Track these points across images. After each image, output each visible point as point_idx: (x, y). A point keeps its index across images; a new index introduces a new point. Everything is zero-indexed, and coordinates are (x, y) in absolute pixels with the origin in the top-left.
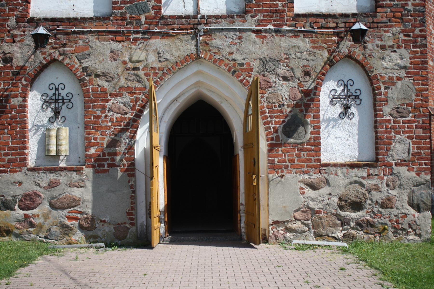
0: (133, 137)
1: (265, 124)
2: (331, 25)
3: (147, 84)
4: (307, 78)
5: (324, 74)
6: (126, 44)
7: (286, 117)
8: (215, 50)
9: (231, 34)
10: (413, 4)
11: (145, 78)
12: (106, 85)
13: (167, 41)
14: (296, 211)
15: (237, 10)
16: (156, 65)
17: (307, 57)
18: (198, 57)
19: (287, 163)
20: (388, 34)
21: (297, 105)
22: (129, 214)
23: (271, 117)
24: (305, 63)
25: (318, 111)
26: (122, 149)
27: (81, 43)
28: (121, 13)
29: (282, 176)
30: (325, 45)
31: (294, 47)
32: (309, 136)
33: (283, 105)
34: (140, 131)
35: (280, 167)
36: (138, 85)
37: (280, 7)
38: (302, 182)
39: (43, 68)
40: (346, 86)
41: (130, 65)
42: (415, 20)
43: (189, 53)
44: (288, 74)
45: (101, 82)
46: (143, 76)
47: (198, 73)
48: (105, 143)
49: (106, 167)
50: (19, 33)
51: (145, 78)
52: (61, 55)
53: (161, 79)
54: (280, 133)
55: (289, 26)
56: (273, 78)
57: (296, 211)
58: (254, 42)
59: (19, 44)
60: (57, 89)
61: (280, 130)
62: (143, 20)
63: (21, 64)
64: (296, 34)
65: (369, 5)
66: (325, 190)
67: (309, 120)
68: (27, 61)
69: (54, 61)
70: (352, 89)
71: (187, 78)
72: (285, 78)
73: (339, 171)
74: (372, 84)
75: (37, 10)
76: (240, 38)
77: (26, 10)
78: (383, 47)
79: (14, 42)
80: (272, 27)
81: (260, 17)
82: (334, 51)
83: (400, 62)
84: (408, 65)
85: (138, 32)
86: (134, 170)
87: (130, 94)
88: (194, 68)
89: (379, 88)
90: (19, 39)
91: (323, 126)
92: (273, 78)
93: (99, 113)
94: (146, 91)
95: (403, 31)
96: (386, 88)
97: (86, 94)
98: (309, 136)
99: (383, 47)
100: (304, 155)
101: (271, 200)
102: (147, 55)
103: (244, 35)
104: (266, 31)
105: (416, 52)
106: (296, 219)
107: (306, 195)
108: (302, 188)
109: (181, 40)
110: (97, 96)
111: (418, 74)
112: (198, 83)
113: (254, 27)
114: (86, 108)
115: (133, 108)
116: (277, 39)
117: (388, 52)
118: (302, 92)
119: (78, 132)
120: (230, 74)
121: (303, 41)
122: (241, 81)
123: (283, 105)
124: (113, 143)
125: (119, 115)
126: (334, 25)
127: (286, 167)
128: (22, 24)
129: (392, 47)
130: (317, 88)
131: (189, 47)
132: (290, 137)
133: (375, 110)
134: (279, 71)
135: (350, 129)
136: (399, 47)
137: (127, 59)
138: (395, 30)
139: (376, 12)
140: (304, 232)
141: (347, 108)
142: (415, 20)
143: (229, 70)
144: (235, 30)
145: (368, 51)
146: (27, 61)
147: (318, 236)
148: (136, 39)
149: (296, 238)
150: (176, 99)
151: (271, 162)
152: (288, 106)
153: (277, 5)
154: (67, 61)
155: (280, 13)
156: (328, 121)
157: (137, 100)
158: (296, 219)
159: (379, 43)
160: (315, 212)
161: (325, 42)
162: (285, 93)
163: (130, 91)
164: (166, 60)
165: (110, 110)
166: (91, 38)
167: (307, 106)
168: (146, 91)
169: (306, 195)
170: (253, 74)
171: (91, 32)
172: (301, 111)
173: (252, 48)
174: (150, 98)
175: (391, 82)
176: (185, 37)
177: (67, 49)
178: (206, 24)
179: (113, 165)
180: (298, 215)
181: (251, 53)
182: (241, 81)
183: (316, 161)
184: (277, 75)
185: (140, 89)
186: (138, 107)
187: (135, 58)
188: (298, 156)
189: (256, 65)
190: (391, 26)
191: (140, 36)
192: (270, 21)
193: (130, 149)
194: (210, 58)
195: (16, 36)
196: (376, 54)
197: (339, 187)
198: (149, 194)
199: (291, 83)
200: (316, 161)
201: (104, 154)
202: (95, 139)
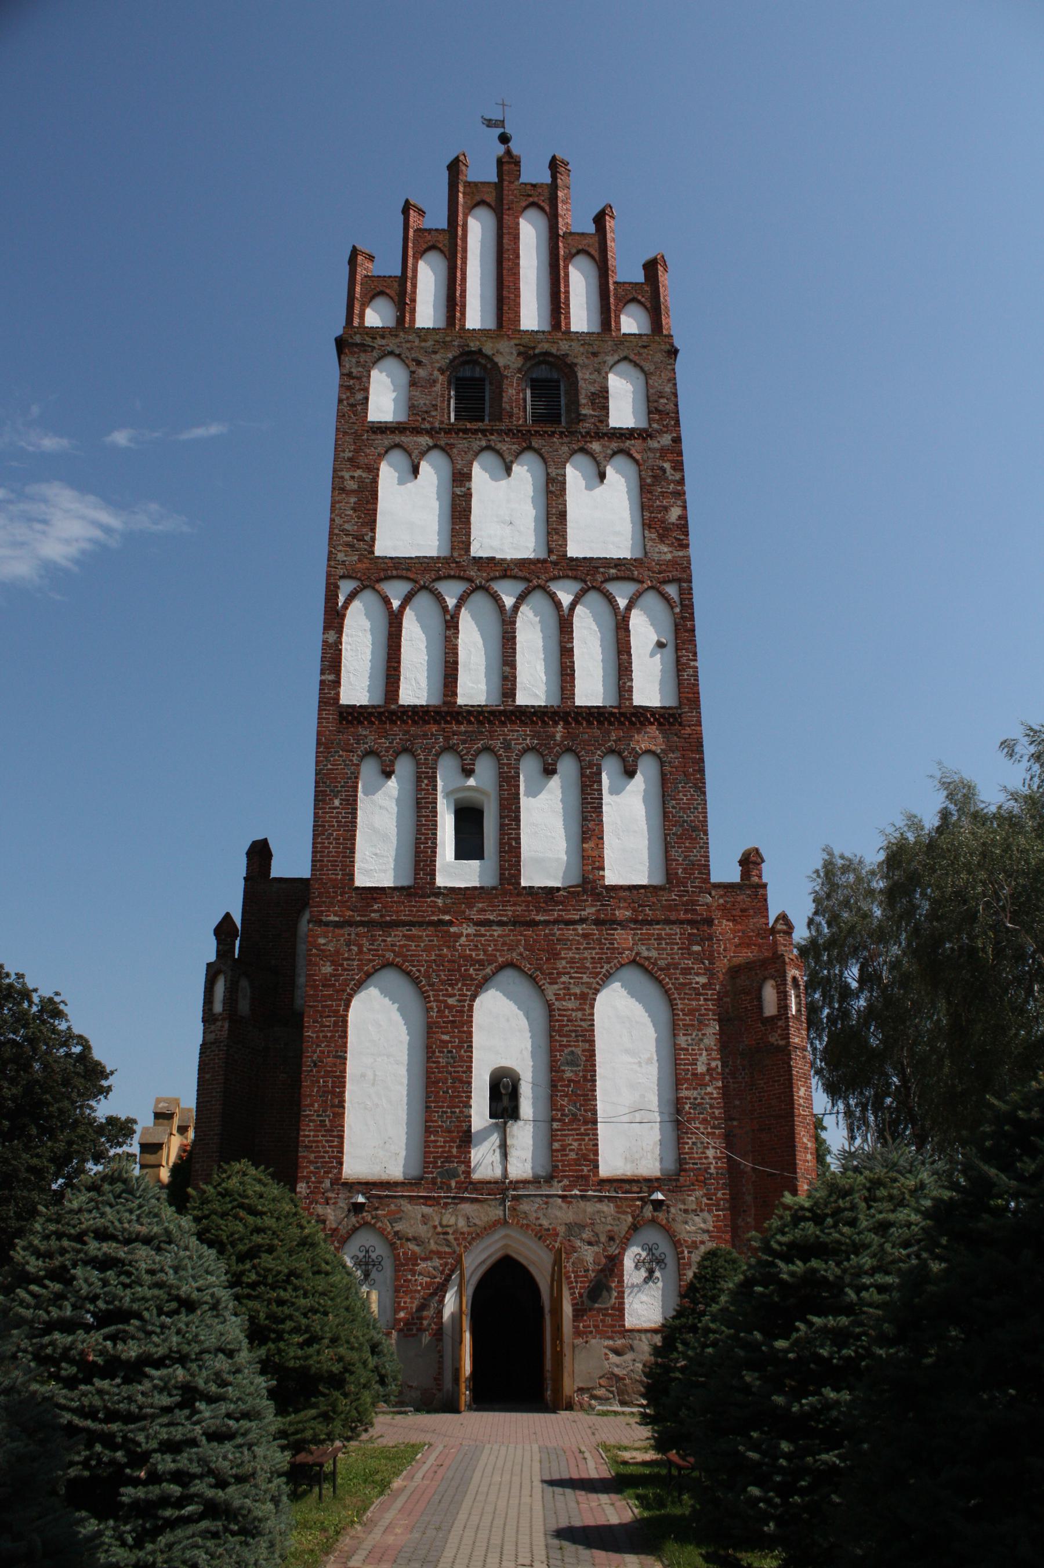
0: (441, 1301)
1: (570, 1289)
2: (635, 1189)
3: (457, 1249)
4: (612, 1243)
5: (628, 1239)
6: (436, 1208)
7: (591, 1282)
8: (523, 1216)
9: (538, 1200)
10: (715, 1168)
11: (454, 1243)
12: (416, 1249)
13: (476, 1206)
14: (600, 1378)
15: (544, 1174)
16: (466, 1229)
17: (612, 1222)
18: (506, 1222)
19: (592, 1329)
20: (691, 1198)
21: (602, 1271)
22: (435, 1379)
23: (576, 1282)
24: (609, 1227)
25: (622, 1276)
26: (430, 1312)
27: (393, 1207)
28: (433, 1178)
29: (587, 1342)
30: (629, 1210)
31: (598, 1212)
32: (613, 1301)
33: (588, 1270)
34: (448, 1296)
35: (585, 1333)
36: (447, 1249)
37: (585, 1172)
38: (606, 1347)
39: (355, 1230)
40: (650, 1250)
41: (439, 1229)
42: (718, 1183)
43: (497, 1218)
44: (593, 1239)
45: (412, 1246)
46: (453, 1241)
47: (506, 1236)
48: (414, 1306)
49: (414, 1331)
50: (333, 1195)
51: (454, 1243)
52: (373, 1218)
53: (470, 1243)
54: (585, 1298)
55: (595, 1191)
56: (578, 1243)
57: (600, 1378)
58: (560, 1208)
59: (332, 1207)
60: (367, 1251)
61: (585, 1295)
62: (453, 1184)
63: (334, 1226)
64: (600, 1199)
65: (673, 1167)
66: (629, 1356)
67: (613, 1285)
68: (340, 1223)
69: (366, 1224)
70: (657, 1253)
71: (496, 1241)
72: (590, 1243)
73: (643, 1337)
74: (676, 1248)
75: (349, 1172)
76: (546, 1203)
77: (340, 1172)
78: (686, 1211)
79: (328, 1204)
80: (578, 1193)
81: (566, 1182)
82: (638, 1216)
83: (702, 1225)
84: (711, 1229)
85: (448, 1197)
86: (441, 1334)
87: (440, 1258)
88: (502, 1232)
89: (683, 1252)
90: (332, 1201)
91: (627, 1291)
92: (578, 1243)
93: (409, 1277)
94: (455, 1256)
95: (705, 1195)
96: (689, 1252)
97: (396, 1257)
98: (613, 1301)
99: (686, 1211)
100: (609, 1320)
101: (576, 1366)
102: (457, 1220)
103: (551, 1200)
104: (572, 1196)
105: (719, 1216)
106: (601, 1386)
107: (611, 1361)
108: (606, 1354)
109: (490, 1206)
110: (407, 1259)
111: (720, 1237)
112: (506, 1246)
113: (560, 1193)
114: (396, 1271)
115: (442, 1272)
116: (582, 1204)
117: (692, 1216)
118: (606, 1257)
119: (326, 1102)
120: (536, 1239)
121: (608, 1206)
122: (547, 1246)
123: (588, 1270)
124: (422, 1307)
125: (428, 1279)
126: (638, 1190)
127: (591, 1332)
128: (335, 1187)
129: (695, 1210)
130: (622, 1254)
131: (497, 1212)
132: (595, 1302)
133: (680, 1275)
134: (584, 1236)
135: (655, 1293)
136: (702, 1210)
137: (437, 1223)
138: (699, 1193)
139: (679, 1175)
140: (609, 1399)
141: (651, 1272)
142: (718, 1183)
143: (536, 1235)
144: (541, 1195)
145: (671, 1216)
146: (340, 1223)
147: (623, 1403)
148: (446, 1204)
149: (600, 1405)
150: (484, 1262)
151: (576, 1328)
152: (593, 1271)
153: (582, 1170)
154: (379, 1224)
155: (586, 1178)
156: (633, 1286)
157: (446, 1264)
158: (601, 1386)
159: (682, 1207)
160: (619, 1379)
161: (630, 1206)
162: (590, 1259)
163: (439, 1254)
164: (475, 1225)
165: (420, 1274)
166: (402, 1202)
167: (612, 1271)
168: (455, 1256)
169: (611, 1361)
170: (559, 1239)
171: (403, 1196)
172: (606, 1276)
173: (558, 1213)
174: (459, 1261)
175: (694, 1246)
176: (493, 1203)
177: (380, 1212)
178: (514, 1190)
179: (421, 1330)
180: (603, 1382)
181: (556, 1218)
182: (547, 1246)
183: (620, 1326)
184: (582, 1240)
185: (449, 1253)
186: (447, 1271)
187: (444, 1223)
188: (603, 1321)
189: (561, 1230)
190: (694, 1190)
191: (449, 1201)
192: (575, 1186)
193: (440, 1313)
194: (517, 1223)
195: (330, 1198)
196: (679, 1219)
197: (643, 1352)
198: (457, 1359)
199: (596, 1249)
200: (620, 1326)
201: (413, 1318)
202: (405, 1303)
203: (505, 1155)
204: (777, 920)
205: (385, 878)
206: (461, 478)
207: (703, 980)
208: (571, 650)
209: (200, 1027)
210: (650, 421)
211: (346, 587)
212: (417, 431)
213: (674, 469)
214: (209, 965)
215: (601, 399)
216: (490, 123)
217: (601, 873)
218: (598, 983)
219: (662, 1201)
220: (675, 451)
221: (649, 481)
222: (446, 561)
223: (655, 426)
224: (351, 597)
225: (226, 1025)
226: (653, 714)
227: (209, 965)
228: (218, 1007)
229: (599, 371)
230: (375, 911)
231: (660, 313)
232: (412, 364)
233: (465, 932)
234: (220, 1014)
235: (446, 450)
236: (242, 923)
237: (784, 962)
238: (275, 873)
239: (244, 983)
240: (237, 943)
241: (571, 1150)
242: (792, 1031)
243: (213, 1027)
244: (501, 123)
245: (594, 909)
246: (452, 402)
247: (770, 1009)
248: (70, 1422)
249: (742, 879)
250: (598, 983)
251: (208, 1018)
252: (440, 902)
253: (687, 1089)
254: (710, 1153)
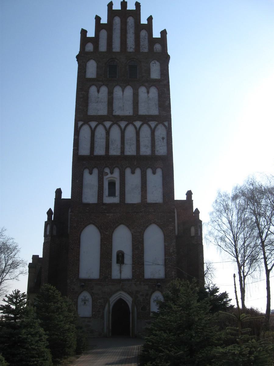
150: (115, 300)
203: (121, 273)
205: (146, 50)
206: (110, 93)
208: (139, 140)
209: (43, 238)
210: (161, 77)
215: (148, 71)
217: (146, 200)
218: (145, 229)
219: (160, 285)
224: (82, 126)
225: (50, 238)
228: (48, 233)
230: (87, 210)
232: (98, 62)
233: (110, 215)
234: (48, 235)
238: (63, 197)
239: (55, 227)
240: (53, 216)
241: (138, 272)
245: (144, 209)
246: (69, 226)
248: (237, 327)
250: (145, 229)
251: (45, 236)
252: (104, 207)
253: (167, 256)
254: (173, 273)
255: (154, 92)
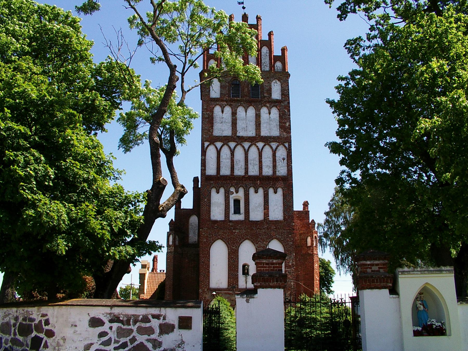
204: (311, 222)
207: (291, 243)
210: (282, 97)
211: (206, 144)
212: (223, 101)
213: (288, 111)
214: (168, 232)
216: (239, 3)
220: (288, 107)
221: (281, 115)
222: (231, 137)
223: (283, 99)
226: (281, 178)
227: (168, 232)
228: (171, 243)
229: (269, 83)
231: (285, 65)
235: (230, 105)
236: (175, 220)
237: (313, 233)
239: (177, 237)
242: (314, 250)
243: (169, 248)
244: (243, 3)
247: (309, 244)
249: (303, 209)
255: (275, 112)
